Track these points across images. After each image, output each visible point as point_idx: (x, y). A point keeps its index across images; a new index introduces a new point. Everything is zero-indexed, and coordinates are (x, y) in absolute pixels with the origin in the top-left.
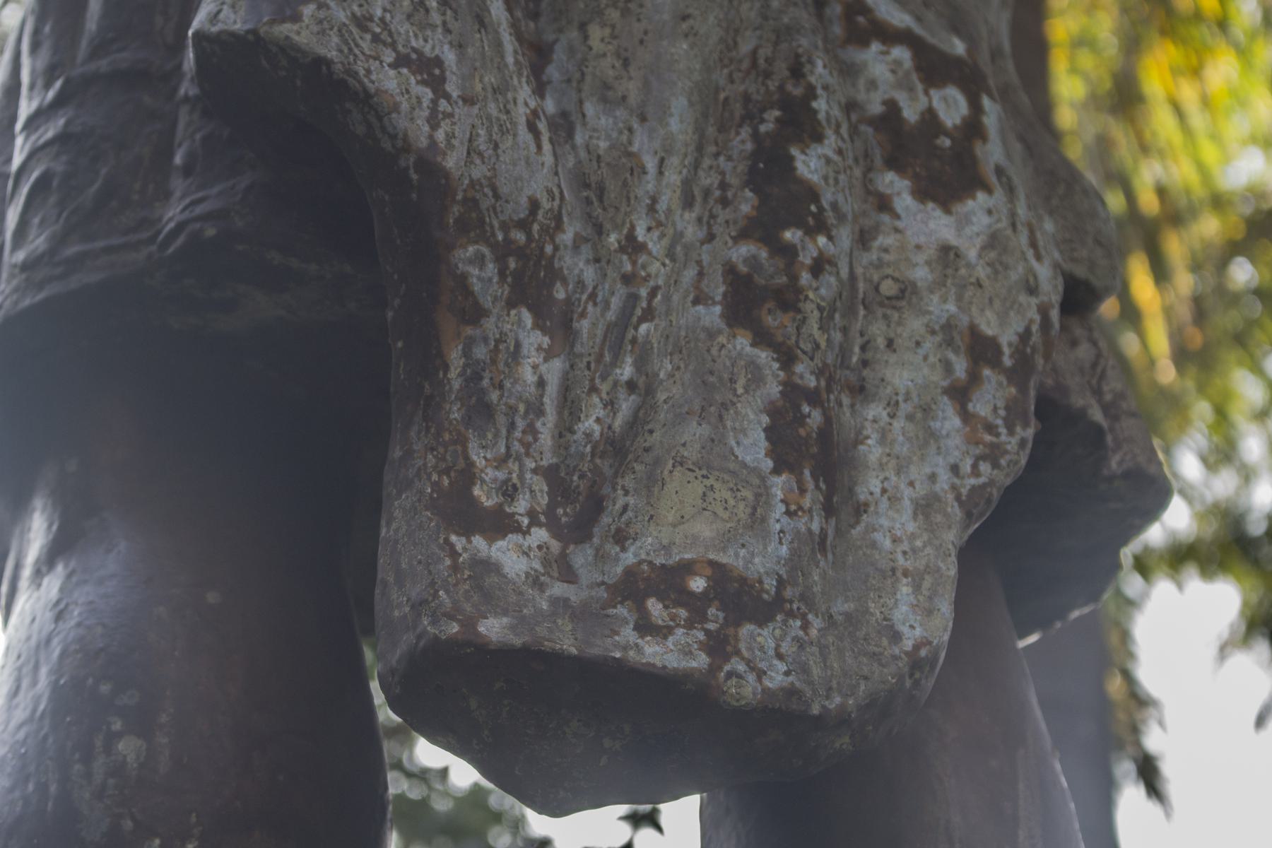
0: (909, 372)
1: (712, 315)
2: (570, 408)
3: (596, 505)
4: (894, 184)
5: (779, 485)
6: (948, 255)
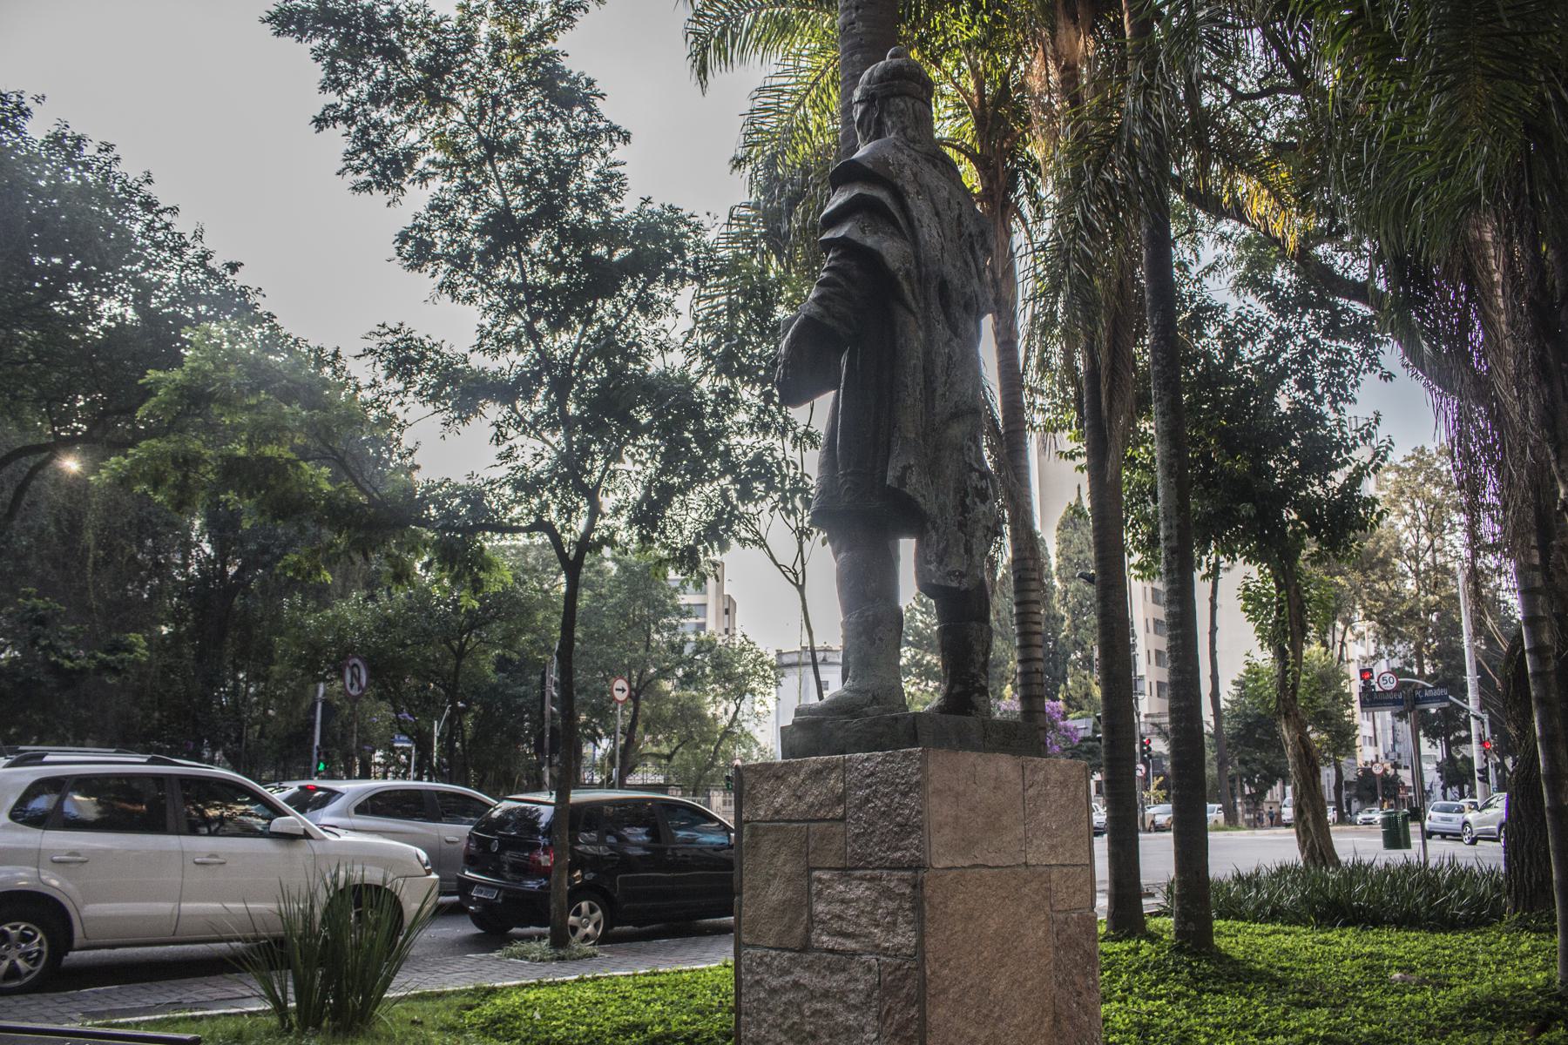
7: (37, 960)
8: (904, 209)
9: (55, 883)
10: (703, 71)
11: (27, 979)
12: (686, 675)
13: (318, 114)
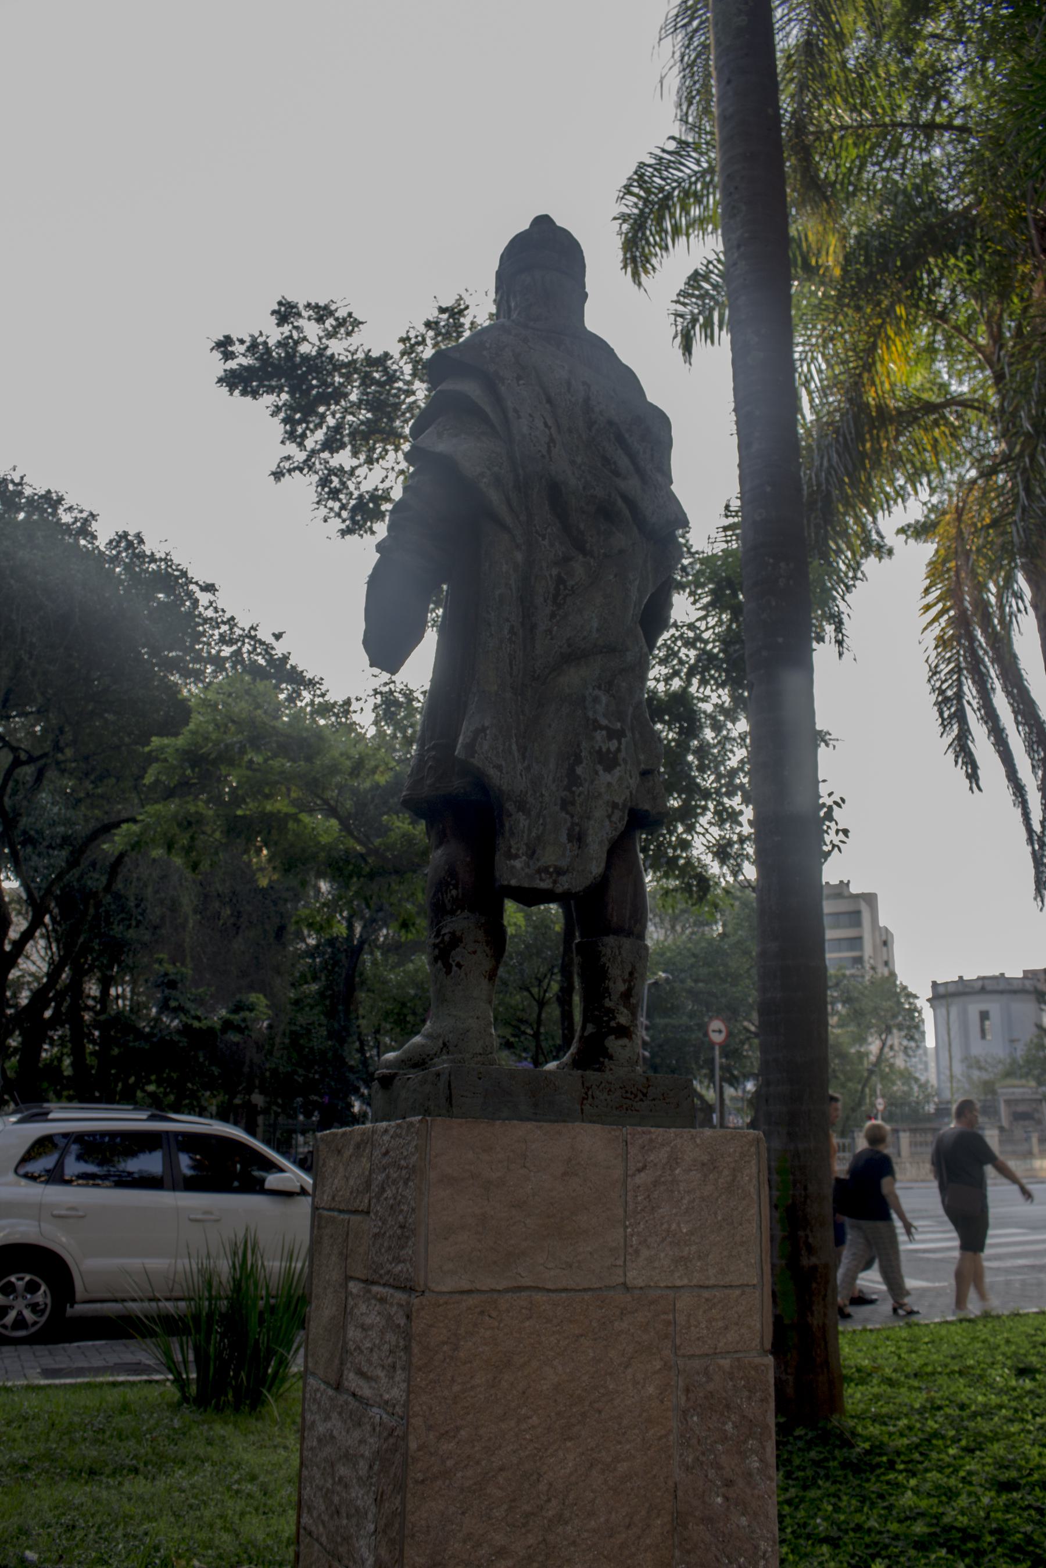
0: (599, 813)
1: (557, 808)
2: (530, 831)
3: (534, 853)
4: (599, 768)
5: (569, 846)
6: (609, 784)
7: (43, 1311)
8: (498, 400)
9: (64, 1239)
10: (687, 348)
11: (33, 1330)
12: (406, 1022)
13: (274, 468)
